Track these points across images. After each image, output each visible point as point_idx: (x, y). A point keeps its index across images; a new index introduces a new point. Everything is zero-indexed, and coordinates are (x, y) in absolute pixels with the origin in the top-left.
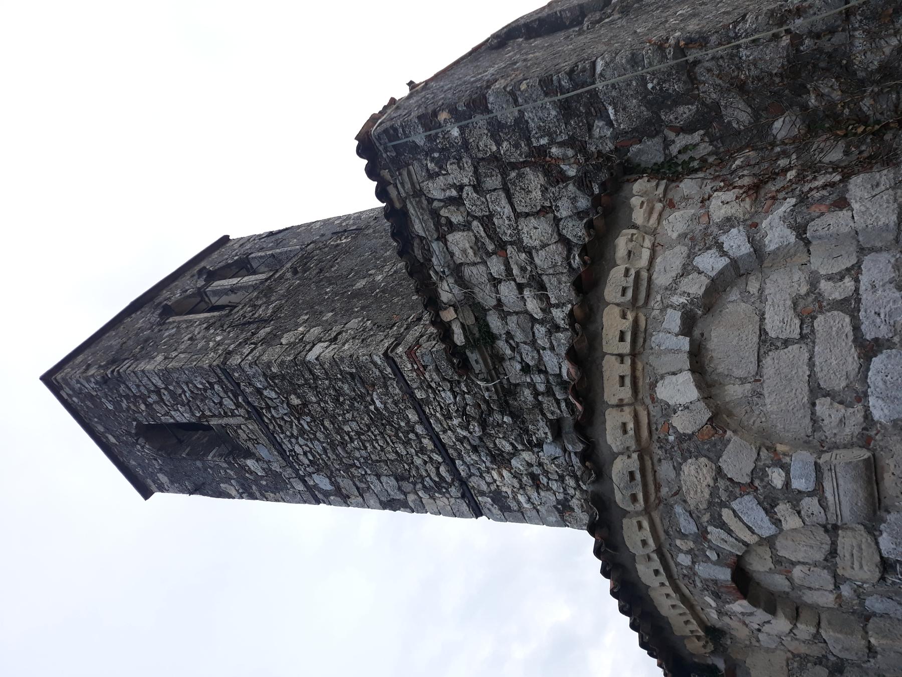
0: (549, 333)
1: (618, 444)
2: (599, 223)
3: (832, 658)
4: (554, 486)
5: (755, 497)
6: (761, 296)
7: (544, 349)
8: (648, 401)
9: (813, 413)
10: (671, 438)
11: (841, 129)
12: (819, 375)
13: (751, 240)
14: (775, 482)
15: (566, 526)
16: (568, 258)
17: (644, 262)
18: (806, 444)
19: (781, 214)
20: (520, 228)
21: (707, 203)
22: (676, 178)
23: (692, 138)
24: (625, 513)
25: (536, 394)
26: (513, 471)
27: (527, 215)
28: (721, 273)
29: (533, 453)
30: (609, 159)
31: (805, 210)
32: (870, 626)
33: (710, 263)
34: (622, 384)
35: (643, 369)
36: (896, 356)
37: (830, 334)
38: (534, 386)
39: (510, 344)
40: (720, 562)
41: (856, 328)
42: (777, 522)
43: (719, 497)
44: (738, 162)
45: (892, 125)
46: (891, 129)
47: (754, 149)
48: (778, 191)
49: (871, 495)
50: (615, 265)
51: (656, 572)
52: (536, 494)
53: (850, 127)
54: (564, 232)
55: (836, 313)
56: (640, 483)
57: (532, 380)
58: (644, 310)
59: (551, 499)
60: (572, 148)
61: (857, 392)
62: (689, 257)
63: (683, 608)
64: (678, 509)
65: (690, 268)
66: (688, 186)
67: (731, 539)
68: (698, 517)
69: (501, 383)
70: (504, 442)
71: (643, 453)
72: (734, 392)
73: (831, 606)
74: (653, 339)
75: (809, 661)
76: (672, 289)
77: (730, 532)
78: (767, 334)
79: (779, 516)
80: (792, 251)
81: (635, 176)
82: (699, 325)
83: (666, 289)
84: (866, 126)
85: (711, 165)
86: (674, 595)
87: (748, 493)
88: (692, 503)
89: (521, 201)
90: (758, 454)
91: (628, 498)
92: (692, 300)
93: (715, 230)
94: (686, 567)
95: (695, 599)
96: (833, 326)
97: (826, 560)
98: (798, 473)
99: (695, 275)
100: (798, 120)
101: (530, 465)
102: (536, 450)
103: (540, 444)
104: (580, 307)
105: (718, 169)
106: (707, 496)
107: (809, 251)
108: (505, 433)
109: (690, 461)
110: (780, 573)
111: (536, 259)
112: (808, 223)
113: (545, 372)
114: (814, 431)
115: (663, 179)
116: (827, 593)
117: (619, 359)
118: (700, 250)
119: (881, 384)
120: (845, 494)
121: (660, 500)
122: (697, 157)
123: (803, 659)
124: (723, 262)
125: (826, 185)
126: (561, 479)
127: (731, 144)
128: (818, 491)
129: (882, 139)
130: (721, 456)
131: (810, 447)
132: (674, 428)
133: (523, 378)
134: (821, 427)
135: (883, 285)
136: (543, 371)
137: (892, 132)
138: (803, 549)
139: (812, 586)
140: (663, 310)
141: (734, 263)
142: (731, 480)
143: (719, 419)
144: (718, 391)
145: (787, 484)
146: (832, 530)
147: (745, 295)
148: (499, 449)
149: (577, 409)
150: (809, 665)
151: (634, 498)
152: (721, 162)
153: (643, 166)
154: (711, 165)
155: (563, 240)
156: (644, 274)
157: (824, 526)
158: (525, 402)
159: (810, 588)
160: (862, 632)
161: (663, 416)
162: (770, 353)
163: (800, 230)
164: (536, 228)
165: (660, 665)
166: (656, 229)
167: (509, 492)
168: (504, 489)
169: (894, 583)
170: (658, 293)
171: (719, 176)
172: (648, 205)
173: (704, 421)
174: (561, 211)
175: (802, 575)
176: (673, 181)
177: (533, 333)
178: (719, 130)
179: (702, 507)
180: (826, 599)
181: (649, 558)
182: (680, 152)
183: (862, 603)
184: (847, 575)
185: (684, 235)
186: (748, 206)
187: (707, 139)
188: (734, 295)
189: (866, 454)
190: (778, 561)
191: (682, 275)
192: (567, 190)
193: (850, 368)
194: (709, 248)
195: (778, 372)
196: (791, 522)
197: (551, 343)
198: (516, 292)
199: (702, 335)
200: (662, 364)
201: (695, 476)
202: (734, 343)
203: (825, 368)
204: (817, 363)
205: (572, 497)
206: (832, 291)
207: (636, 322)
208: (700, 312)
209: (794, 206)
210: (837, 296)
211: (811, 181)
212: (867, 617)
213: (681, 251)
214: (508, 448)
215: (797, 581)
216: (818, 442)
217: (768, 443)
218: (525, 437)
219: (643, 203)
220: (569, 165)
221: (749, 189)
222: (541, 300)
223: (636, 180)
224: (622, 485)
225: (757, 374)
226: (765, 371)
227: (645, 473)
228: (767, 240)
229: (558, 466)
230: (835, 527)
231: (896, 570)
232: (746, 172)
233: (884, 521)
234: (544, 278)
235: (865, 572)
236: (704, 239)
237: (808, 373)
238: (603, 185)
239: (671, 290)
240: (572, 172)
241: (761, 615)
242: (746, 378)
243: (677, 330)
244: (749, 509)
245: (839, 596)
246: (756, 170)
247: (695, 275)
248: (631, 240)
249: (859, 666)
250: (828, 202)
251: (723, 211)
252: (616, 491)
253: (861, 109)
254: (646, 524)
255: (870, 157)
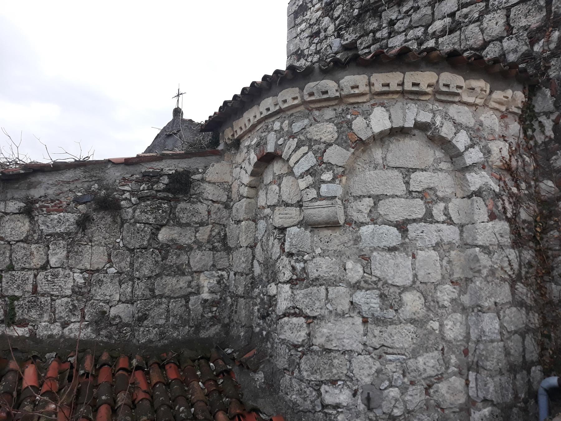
0: (417, 39)
1: (345, 83)
2: (497, 68)
3: (232, 204)
4: (313, 48)
5: (315, 165)
6: (436, 170)
7: (406, 35)
8: (372, 102)
9: (364, 196)
10: (349, 117)
11: (540, 219)
12: (387, 200)
13: (474, 165)
14: (325, 175)
15: (288, 57)
16: (471, 49)
17: (465, 98)
18: (347, 193)
19: (489, 183)
20: (499, 11)
21: (502, 139)
22: (522, 120)
23: (549, 131)
24: (302, 89)
25: (374, 32)
26: (321, 18)
27: (508, 16)
28: (454, 147)
29: (334, 32)
30: (543, 74)
31: (490, 197)
32: (251, 222)
33: (461, 140)
34: (383, 85)
35: (393, 99)
36: (397, 239)
37: (411, 206)
38: (380, 30)
39: (410, 10)
40: (277, 146)
41: (414, 221)
42: (302, 176)
43: (314, 145)
44: (527, 159)
45: (538, 246)
46: (536, 246)
47: (535, 169)
48: (505, 182)
49: (319, 224)
50: (465, 79)
51: (268, 109)
52: (307, 35)
53: (541, 224)
54: (491, 45)
55: (424, 210)
56: (321, 98)
57: (384, 28)
58: (433, 99)
59: (304, 45)
60: (556, 47)
61: (376, 219)
62: (467, 127)
63: (248, 126)
64: (306, 121)
65: (459, 127)
66: (515, 127)
67: (291, 152)
68: (302, 133)
69: (383, 5)
70: (340, 11)
71: (340, 99)
72: (378, 153)
73: (258, 204)
74: (413, 105)
75: (228, 193)
76: (446, 116)
77: (294, 151)
78: (413, 172)
79: (305, 177)
80: (465, 188)
81: (527, 93)
82: (421, 133)
83: (446, 113)
84: (540, 233)
85: (527, 142)
86: (256, 120)
87: (317, 161)
88: (310, 129)
89: (520, 10)
90: (340, 167)
91: (311, 90)
92: (437, 129)
93: (483, 144)
94: (273, 127)
95: (254, 132)
96: (417, 208)
97: (283, 201)
98: (330, 187)
99: (454, 130)
100: (551, 195)
101: (325, 30)
102: (336, 34)
103: (339, 36)
104: (438, 56)
105: (524, 146)
106: (315, 138)
107: (464, 198)
108: (346, 11)
109: (335, 128)
110: (274, 178)
111: (473, 25)
112: (482, 198)
113: (389, 37)
114: (354, 197)
115: (522, 111)
116: (265, 201)
117: (400, 83)
118: (470, 134)
119: (381, 231)
120: (320, 212)
121: (311, 110)
122: (535, 134)
123: (229, 190)
124: (461, 148)
125: (505, 209)
126: (317, 52)
127: (541, 155)
128: (320, 197)
129: (530, 240)
130: (338, 146)
131: (344, 194)
132: (356, 118)
133: (385, 21)
134: (356, 200)
135: (439, 236)
136: (390, 35)
137: (534, 246)
138: (288, 189)
139: (268, 194)
140: (432, 111)
141: (460, 155)
142: (325, 151)
143: (361, 145)
144: (378, 145)
145: (324, 182)
146: (300, 204)
147: (438, 161)
148: (335, 7)
149: (367, 56)
150: (227, 193)
151: (312, 94)
152: (529, 149)
153: (534, 98)
154: (527, 142)
155: (486, 44)
156: (457, 99)
157: (301, 201)
158: (368, 23)
159: (267, 193)
160: (247, 218)
161: (363, 111)
162: (401, 174)
163: (478, 193)
164: (497, 23)
165: (215, 113)
166: (488, 106)
167: (307, 17)
168: (309, 13)
169: (274, 233)
170: (444, 108)
171: (519, 147)
172: (505, 101)
173: (359, 136)
174: (508, 42)
175: (274, 190)
176: (520, 118)
177: (418, 27)
178: (552, 148)
179: (309, 136)
180: (262, 201)
181: (276, 105)
182: (540, 122)
183: (261, 218)
184: (275, 211)
185: (481, 125)
186: (497, 164)
187: (547, 140)
188: (439, 154)
189: (342, 222)
190: (280, 177)
191: (455, 123)
192: (523, 45)
193: (390, 216)
194: (471, 140)
195: (390, 178)
196: (303, 184)
197: (410, 40)
198: (449, 12)
199: (414, 135)
200: (397, 110)
201: (326, 131)
202: (408, 154)
203: (391, 203)
204: (394, 199)
205: (306, 60)
206: (438, 210)
207: (426, 94)
208: (429, 133)
209: (494, 191)
210: (435, 212)
211: (509, 200)
212: (255, 220)
213: (471, 123)
214: (336, 14)
215: (270, 187)
216: (346, 199)
217: (346, 172)
218: (343, 26)
219: (507, 98)
220: (543, 46)
221: (508, 165)
222: (442, 31)
223: (524, 93)
224: (319, 86)
225: (388, 166)
226: (390, 171)
227: (327, 101)
228: (473, 174)
229: (326, 49)
230: (301, 206)
231: (280, 234)
232: (520, 163)
233: (306, 229)
234: (458, 32)
235: (278, 219)
236: (477, 136)
237: (388, 194)
238: (524, 70)
239: (445, 116)
240: (537, 48)
241: (250, 169)
242: (386, 160)
243: (418, 119)
244: (309, 161)
245: (264, 208)
246: (520, 169)
247: (454, 131)
248: (482, 90)
249: (229, 216)
250: (494, 209)
251: (495, 148)
252: (315, 83)
253: (551, 230)
254: (296, 102)
255: (519, 234)
